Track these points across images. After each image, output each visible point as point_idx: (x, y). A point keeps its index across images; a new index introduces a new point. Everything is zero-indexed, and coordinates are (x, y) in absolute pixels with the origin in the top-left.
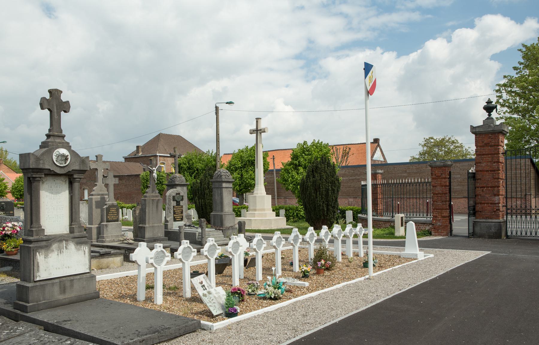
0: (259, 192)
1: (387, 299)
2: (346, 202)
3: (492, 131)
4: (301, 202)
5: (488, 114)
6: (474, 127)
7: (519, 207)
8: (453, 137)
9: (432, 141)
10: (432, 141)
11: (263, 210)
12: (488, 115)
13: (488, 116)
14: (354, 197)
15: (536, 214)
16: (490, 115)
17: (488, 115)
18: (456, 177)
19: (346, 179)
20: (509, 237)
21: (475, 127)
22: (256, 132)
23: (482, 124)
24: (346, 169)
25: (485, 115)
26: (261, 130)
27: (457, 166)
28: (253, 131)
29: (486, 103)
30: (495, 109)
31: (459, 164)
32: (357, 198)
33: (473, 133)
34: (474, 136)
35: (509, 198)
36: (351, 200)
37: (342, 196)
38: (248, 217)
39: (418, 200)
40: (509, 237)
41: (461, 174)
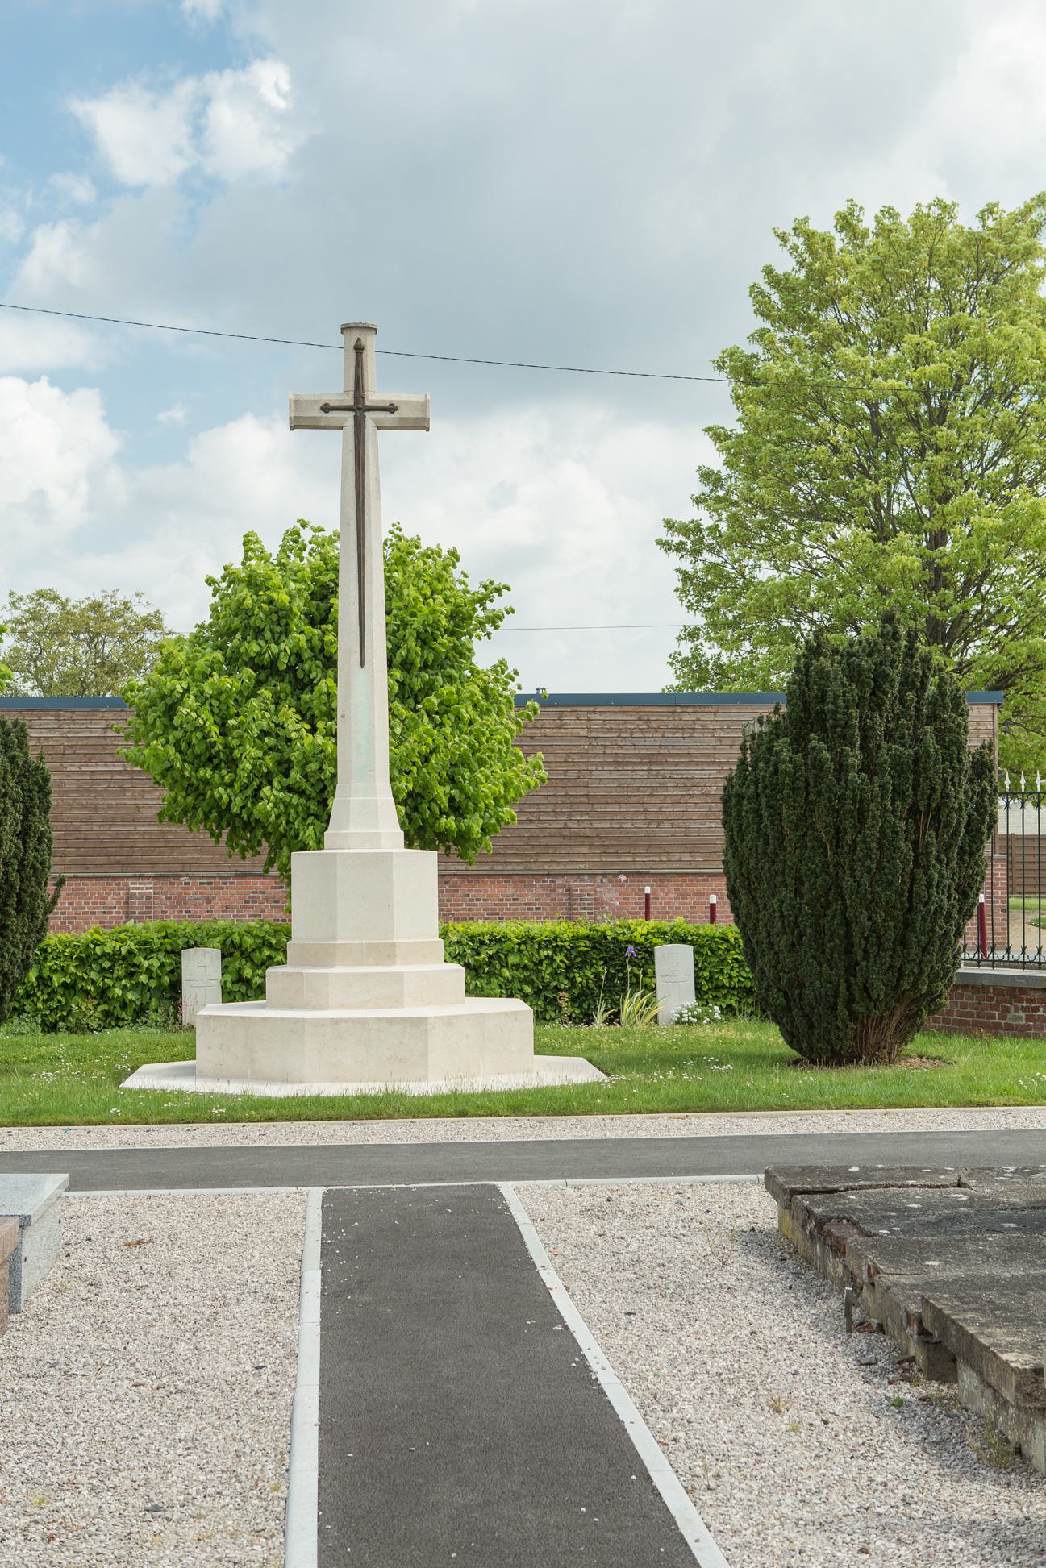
0: (381, 830)
1: (670, 1521)
2: (111, 901)
8: (143, 599)
9: (53, 608)
10: (53, 608)
11: (386, 953)
14: (161, 870)
18: (698, 774)
19: (112, 773)
22: (349, 418)
24: (108, 715)
26: (392, 409)
27: (704, 727)
28: (326, 408)
31: (712, 717)
32: (177, 877)
36: (142, 889)
37: (86, 866)
38: (342, 1006)
41: (720, 763)
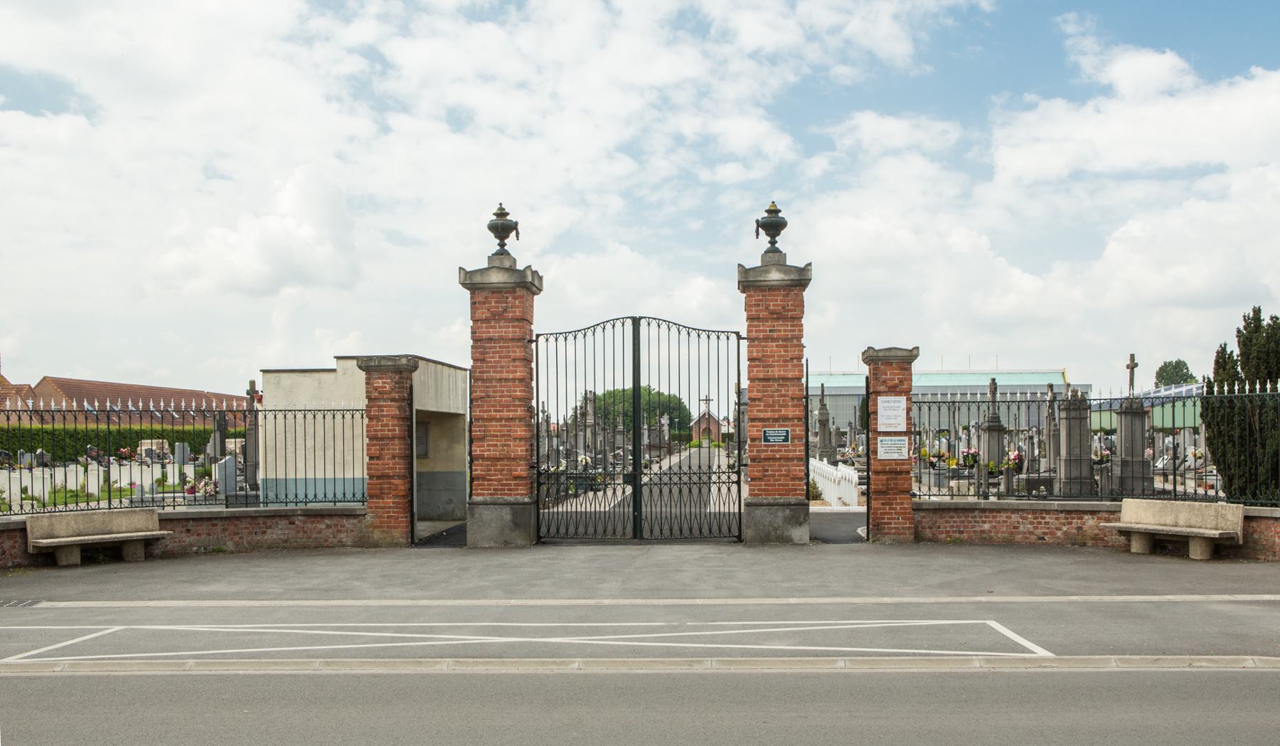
3: (781, 282)
4: (99, 556)
5: (498, 241)
6: (467, 273)
7: (676, 469)
12: (769, 242)
13: (499, 248)
15: (729, 483)
16: (502, 245)
17: (769, 242)
20: (542, 540)
21: (750, 269)
23: (760, 265)
25: (492, 244)
29: (767, 211)
30: (515, 231)
33: (464, 285)
34: (467, 293)
35: (1137, 477)
39: (330, 475)
40: (542, 540)
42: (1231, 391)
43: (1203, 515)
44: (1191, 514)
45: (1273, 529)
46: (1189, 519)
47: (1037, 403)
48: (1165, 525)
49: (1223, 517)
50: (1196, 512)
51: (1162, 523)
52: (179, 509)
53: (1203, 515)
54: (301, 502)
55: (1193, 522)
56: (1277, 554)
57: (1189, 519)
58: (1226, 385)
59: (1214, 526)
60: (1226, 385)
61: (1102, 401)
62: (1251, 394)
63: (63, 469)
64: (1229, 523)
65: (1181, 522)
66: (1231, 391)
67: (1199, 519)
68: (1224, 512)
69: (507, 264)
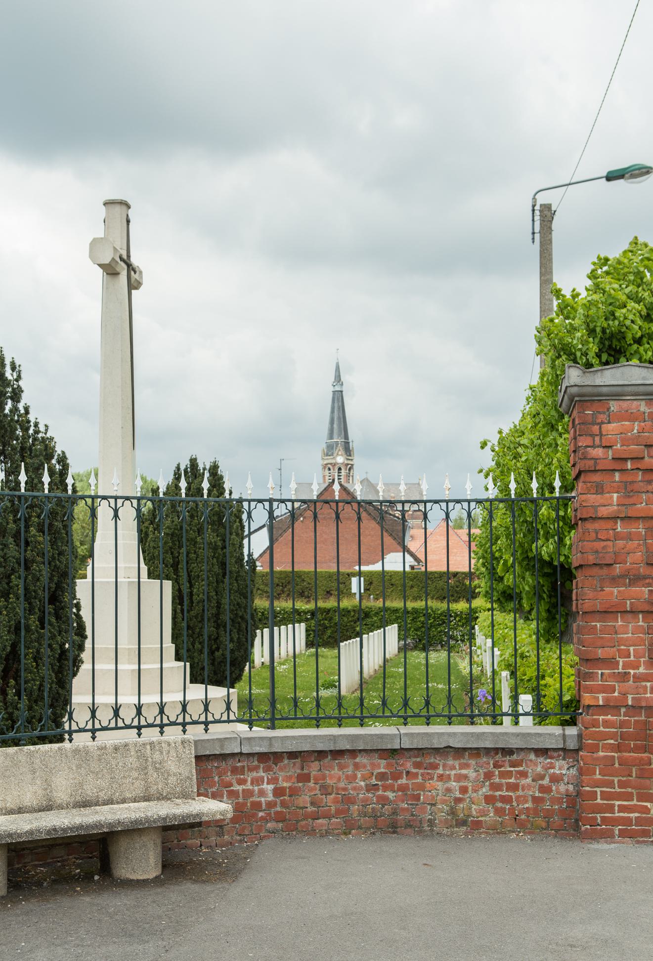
42: (34, 484)
43: (111, 770)
44: (83, 771)
45: (216, 779)
46: (81, 785)
47: (267, 504)
48: (20, 811)
49: (159, 767)
50: (95, 766)
51: (9, 805)
52: (217, 731)
53: (111, 770)
54: (81, 730)
55: (90, 790)
56: (226, 828)
57: (81, 785)
58: (535, 491)
59: (139, 792)
60: (535, 491)
61: (297, 505)
62: (53, 494)
63: (385, 569)
64: (172, 780)
65: (61, 795)
66: (34, 484)
67: (104, 783)
68: (157, 756)
69: (627, 176)
